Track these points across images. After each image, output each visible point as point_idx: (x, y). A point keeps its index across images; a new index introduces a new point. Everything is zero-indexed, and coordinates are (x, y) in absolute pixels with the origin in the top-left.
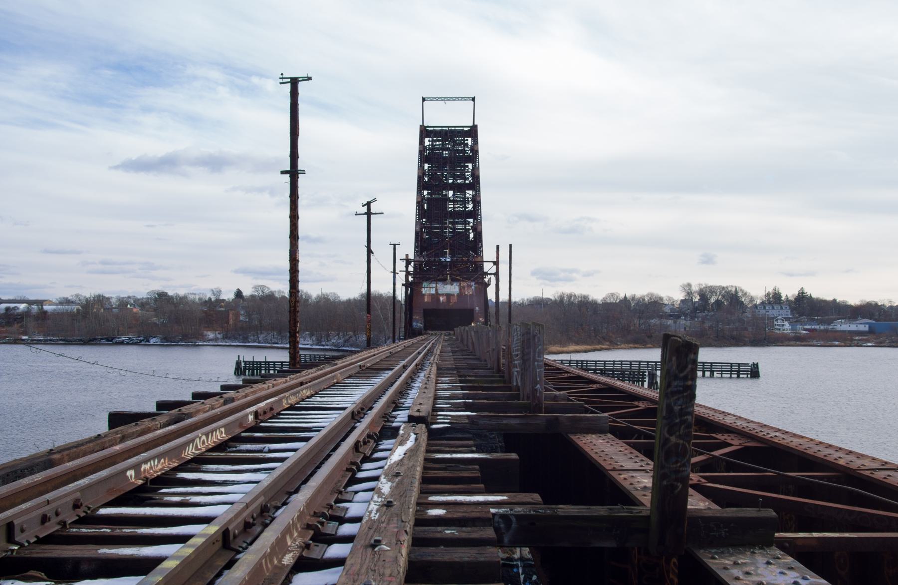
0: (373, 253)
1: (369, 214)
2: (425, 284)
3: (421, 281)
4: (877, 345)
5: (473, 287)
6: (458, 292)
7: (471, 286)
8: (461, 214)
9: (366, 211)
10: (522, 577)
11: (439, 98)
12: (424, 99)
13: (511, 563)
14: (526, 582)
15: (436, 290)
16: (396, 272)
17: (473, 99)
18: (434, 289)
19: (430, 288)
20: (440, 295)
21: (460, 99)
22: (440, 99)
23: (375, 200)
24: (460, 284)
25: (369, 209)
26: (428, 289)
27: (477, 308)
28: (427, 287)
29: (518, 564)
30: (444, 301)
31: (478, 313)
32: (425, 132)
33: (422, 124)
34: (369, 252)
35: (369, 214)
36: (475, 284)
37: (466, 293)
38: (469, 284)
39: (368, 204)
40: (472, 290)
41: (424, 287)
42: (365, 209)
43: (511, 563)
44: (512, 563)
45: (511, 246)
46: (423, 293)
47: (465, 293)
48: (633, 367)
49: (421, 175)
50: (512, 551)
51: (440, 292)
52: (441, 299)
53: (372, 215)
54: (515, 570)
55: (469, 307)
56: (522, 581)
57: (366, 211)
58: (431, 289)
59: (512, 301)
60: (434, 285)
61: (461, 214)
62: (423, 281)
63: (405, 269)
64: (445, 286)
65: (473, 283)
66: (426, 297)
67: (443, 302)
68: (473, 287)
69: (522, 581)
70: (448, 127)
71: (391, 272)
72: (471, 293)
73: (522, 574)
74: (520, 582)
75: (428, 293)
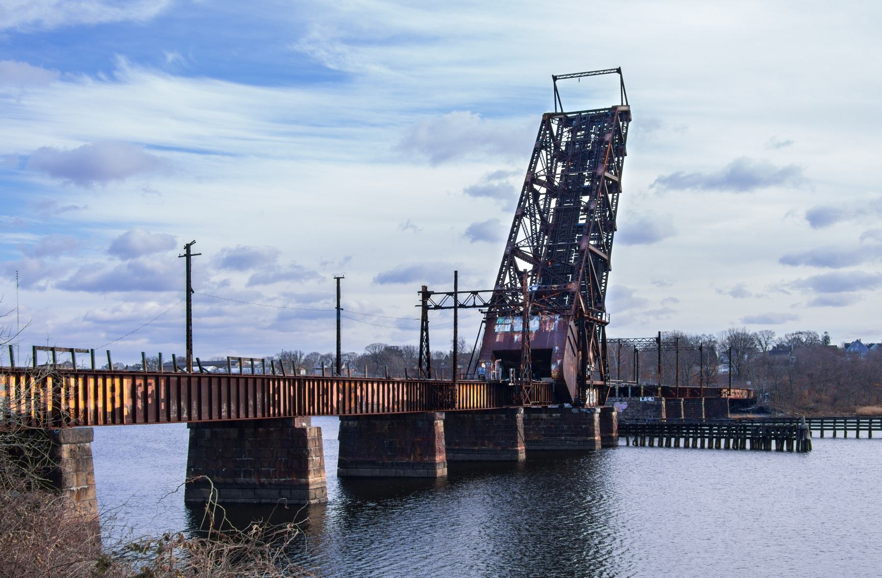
0: (193, 292)
1: (188, 256)
4: (292, 368)
5: (557, 322)
6: (538, 328)
7: (554, 320)
9: (186, 253)
11: (574, 74)
12: (555, 78)
17: (619, 71)
18: (510, 325)
19: (506, 324)
20: (515, 332)
21: (602, 72)
23: (194, 242)
27: (557, 348)
30: (519, 340)
31: (557, 353)
34: (189, 291)
35: (188, 256)
36: (559, 317)
39: (188, 247)
40: (555, 325)
41: (498, 324)
45: (200, 254)
46: (496, 331)
48: (861, 426)
53: (421, 304)
55: (547, 346)
57: (186, 253)
58: (506, 326)
59: (607, 337)
65: (557, 317)
66: (498, 336)
67: (517, 341)
68: (557, 322)
72: (552, 329)
75: (501, 330)
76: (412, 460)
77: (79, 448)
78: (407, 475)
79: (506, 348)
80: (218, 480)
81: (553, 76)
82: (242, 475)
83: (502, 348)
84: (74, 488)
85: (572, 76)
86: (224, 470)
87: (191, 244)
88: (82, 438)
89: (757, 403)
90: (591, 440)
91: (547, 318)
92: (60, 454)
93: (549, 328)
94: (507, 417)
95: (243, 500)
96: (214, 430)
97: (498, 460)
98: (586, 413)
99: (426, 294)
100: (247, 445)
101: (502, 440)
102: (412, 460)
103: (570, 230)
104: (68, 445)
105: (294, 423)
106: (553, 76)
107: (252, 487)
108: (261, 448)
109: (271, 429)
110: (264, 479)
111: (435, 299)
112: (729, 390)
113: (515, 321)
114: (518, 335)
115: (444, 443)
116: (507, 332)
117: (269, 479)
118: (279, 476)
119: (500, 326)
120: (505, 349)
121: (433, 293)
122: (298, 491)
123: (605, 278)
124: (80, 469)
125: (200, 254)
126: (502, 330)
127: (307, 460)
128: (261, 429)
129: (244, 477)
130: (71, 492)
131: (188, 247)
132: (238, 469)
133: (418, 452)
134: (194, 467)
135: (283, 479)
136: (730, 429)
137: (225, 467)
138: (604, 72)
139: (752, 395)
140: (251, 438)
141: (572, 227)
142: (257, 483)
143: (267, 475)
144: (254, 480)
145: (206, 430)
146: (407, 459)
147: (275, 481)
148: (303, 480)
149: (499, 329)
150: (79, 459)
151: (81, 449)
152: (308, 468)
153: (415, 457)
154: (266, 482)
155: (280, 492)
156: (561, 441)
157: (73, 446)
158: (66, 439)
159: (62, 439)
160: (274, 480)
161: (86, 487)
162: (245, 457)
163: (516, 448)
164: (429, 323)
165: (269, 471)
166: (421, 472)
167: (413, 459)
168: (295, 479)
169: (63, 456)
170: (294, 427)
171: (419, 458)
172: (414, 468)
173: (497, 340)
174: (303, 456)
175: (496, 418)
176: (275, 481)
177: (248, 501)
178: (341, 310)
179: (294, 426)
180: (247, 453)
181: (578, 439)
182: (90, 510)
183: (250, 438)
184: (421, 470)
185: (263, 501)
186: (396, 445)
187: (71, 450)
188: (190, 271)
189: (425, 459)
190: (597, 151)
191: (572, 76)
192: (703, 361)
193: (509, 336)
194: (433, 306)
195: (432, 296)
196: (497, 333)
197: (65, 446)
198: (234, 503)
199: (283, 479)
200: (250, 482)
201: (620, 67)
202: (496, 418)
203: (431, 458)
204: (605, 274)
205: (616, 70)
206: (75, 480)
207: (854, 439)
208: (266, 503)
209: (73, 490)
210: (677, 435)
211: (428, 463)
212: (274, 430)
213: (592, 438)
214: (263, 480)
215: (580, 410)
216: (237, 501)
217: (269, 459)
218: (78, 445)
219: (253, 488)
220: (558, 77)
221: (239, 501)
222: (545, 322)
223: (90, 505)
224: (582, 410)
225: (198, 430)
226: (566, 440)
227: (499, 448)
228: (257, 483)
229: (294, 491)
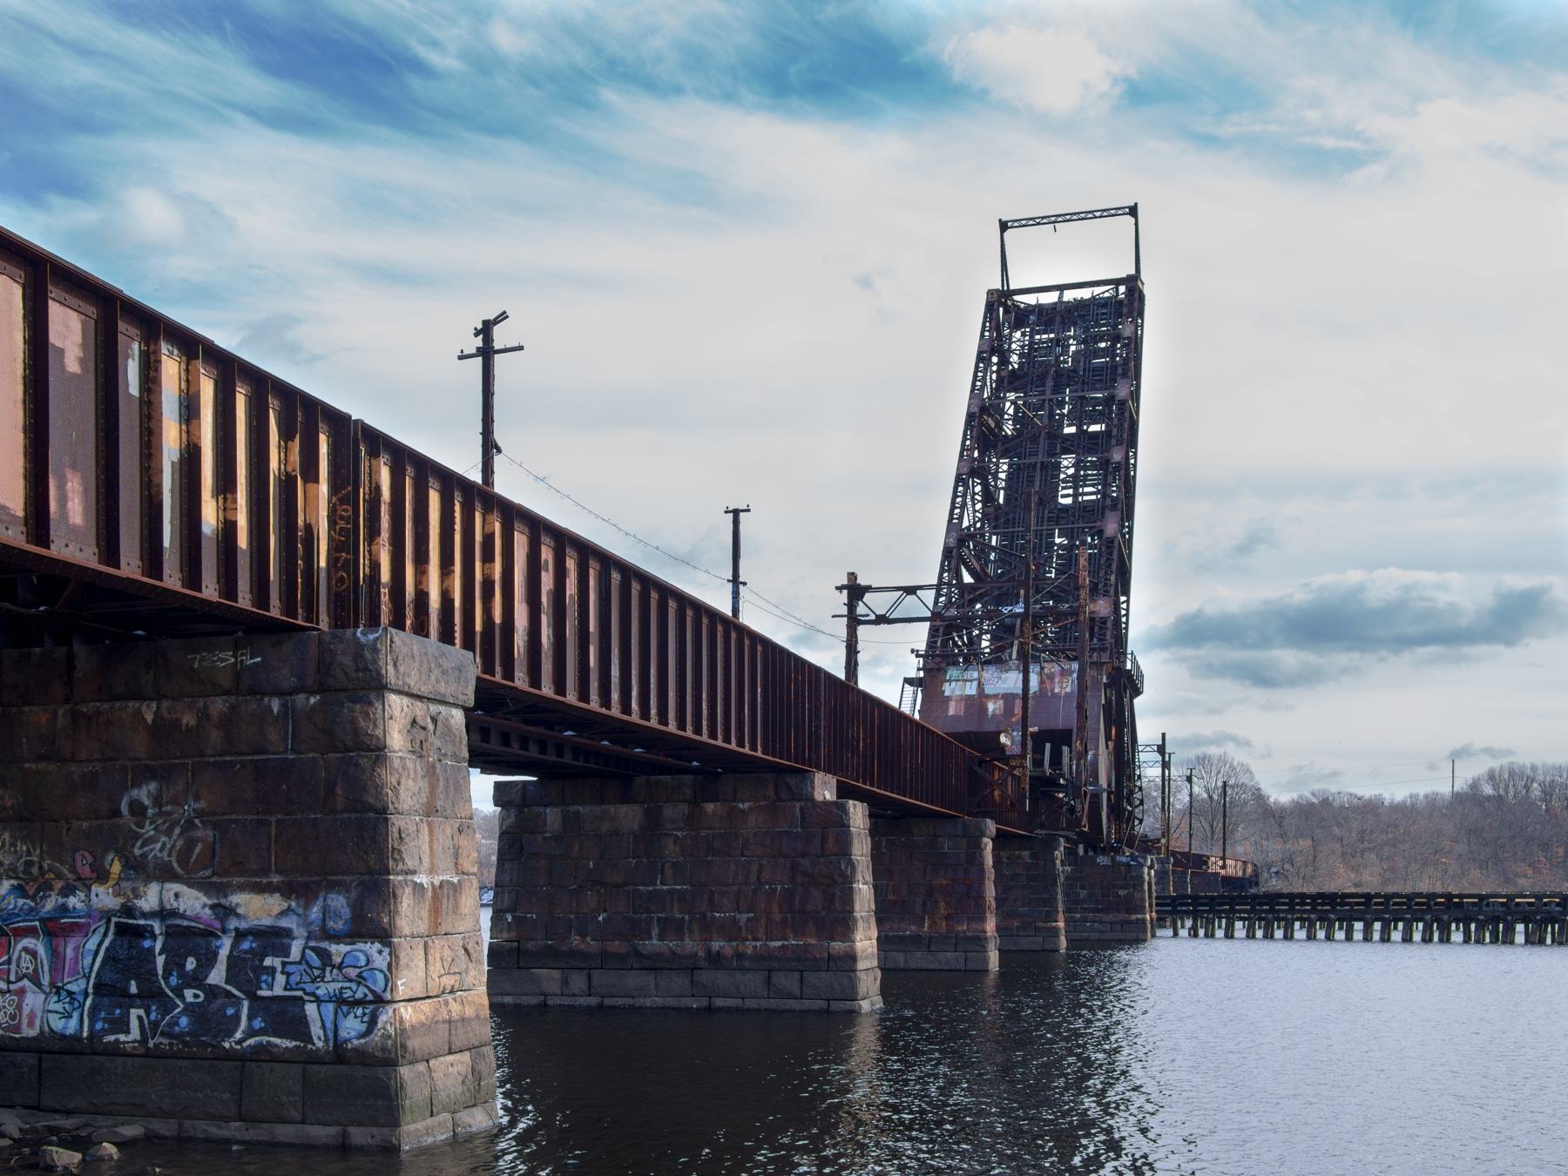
0: (499, 451)
1: (487, 353)
2: (952, 672)
3: (943, 665)
8: (1093, 510)
10: (160, 961)
11: (1043, 218)
12: (1004, 226)
13: (131, 921)
14: (171, 975)
15: (980, 685)
16: (741, 580)
17: (1133, 211)
18: (975, 684)
19: (967, 681)
20: (988, 697)
21: (1098, 214)
22: (1045, 221)
23: (503, 316)
24: (1042, 668)
25: (488, 339)
26: (961, 683)
28: (957, 681)
29: (152, 926)
30: (997, 712)
32: (1000, 302)
33: (997, 285)
35: (487, 353)
37: (1057, 690)
38: (1067, 667)
39: (486, 330)
41: (950, 681)
42: (479, 342)
43: (131, 921)
44: (135, 922)
45: (520, 348)
46: (946, 694)
47: (1052, 690)
49: (976, 410)
50: (134, 890)
51: (988, 690)
52: (991, 706)
53: (846, 613)
54: (147, 944)
56: (160, 972)
58: (968, 684)
60: (975, 675)
61: (1093, 510)
62: (948, 665)
63: (844, 611)
64: (1004, 676)
66: (952, 705)
67: (994, 715)
69: (160, 972)
70: (1061, 288)
71: (729, 581)
72: (1068, 690)
73: (160, 954)
74: (157, 975)
75: (958, 693)
76: (926, 929)
77: (434, 720)
78: (913, 965)
79: (972, 728)
80: (582, 947)
81: (1000, 220)
82: (655, 932)
83: (961, 729)
84: (422, 879)
85: (1038, 220)
86: (600, 919)
87: (496, 321)
88: (447, 683)
89: (1261, 885)
90: (1137, 920)
91: (1053, 667)
92: (379, 732)
93: (1061, 688)
94: (1033, 856)
95: (659, 1001)
96: (573, 809)
97: (1013, 948)
98: (1128, 865)
99: (855, 591)
100: (671, 849)
101: (1023, 906)
102: (926, 929)
103: (1043, 518)
104: (406, 700)
105: (813, 788)
106: (1000, 220)
107: (689, 966)
108: (710, 858)
109: (741, 806)
110: (722, 944)
111: (875, 603)
112: (1223, 859)
113: (985, 674)
114: (995, 703)
115: (994, 894)
116: (969, 697)
117: (734, 943)
118: (766, 934)
119: (953, 684)
120: (969, 729)
121: (868, 589)
122: (823, 974)
123: (1124, 606)
124: (439, 804)
125: (520, 348)
126: (959, 693)
127: (851, 889)
128: (710, 807)
129: (661, 938)
130: (414, 889)
131: (486, 330)
132: (644, 916)
133: (943, 909)
134: (512, 910)
135: (779, 944)
136: (1432, 903)
137: (605, 911)
138: (1106, 213)
139: (1249, 870)
140: (682, 829)
141: (1046, 511)
142: (701, 954)
143: (732, 931)
144: (690, 945)
145: (548, 810)
146: (913, 928)
147: (755, 947)
148: (838, 946)
149: (953, 690)
150: (434, 767)
151: (439, 724)
152: (852, 911)
153: (933, 923)
154: (728, 951)
155: (769, 978)
156: (1075, 921)
157: (420, 709)
158: (402, 669)
159: (390, 668)
160: (749, 947)
161: (455, 880)
162: (663, 883)
163: (1054, 924)
164: (859, 655)
165: (735, 922)
166: (950, 958)
167: (930, 927)
168: (813, 941)
169: (389, 741)
170: (812, 800)
171: (944, 925)
172: (932, 949)
173: (951, 712)
174: (840, 880)
175: (1008, 858)
176: (755, 947)
177: (672, 1002)
178: (741, 586)
179: (812, 794)
180: (669, 872)
181: (1111, 917)
182: (467, 971)
183: (678, 829)
184: (949, 954)
185: (719, 1002)
186: (886, 896)
187: (414, 721)
188: (493, 394)
189: (960, 928)
190: (1084, 370)
191: (1036, 221)
192: (429, 979)
193: (976, 704)
194: (873, 617)
195: (868, 597)
196: (948, 699)
197: (393, 699)
198: (633, 1008)
199: (779, 944)
200: (679, 951)
201: (1136, 204)
202: (1008, 858)
203: (974, 926)
204: (1123, 599)
205: (1127, 210)
206: (426, 848)
207: (1459, 944)
208: (728, 1010)
209: (421, 885)
210: (1289, 916)
211: (967, 938)
212: (750, 808)
213: (1139, 916)
214: (716, 945)
215: (1113, 859)
216: (639, 1002)
217: (736, 888)
218: (434, 708)
219: (687, 968)
220: (1009, 224)
221: (648, 1002)
222: (1051, 677)
223: (466, 950)
224: (1119, 858)
225: (526, 810)
226: (1085, 920)
227: (1016, 924)
228: (701, 954)
229: (810, 977)
